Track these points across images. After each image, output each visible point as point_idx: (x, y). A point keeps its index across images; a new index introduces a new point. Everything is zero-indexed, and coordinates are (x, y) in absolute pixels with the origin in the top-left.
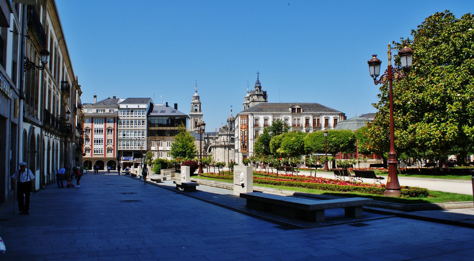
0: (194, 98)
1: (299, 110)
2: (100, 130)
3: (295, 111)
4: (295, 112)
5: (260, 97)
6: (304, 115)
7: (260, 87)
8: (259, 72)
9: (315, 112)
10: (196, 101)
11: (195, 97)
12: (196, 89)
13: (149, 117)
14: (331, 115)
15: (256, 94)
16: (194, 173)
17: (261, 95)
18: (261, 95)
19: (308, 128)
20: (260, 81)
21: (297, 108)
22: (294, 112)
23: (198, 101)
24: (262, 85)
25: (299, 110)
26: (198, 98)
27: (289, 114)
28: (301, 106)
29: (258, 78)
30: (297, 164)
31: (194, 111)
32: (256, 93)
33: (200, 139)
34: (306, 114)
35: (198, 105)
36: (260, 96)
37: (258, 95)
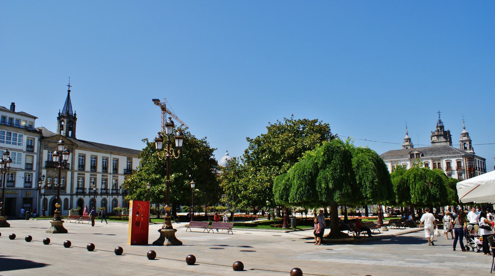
2: (482, 171)
5: (440, 138)
7: (442, 127)
8: (440, 111)
10: (408, 143)
11: (463, 134)
13: (30, 186)
14: (453, 157)
16: (257, 214)
18: (441, 135)
19: (450, 172)
20: (442, 120)
21: (416, 154)
23: (467, 138)
26: (467, 134)
27: (407, 160)
29: (439, 118)
31: (463, 149)
32: (436, 133)
33: (46, 194)
35: (468, 143)
36: (440, 136)
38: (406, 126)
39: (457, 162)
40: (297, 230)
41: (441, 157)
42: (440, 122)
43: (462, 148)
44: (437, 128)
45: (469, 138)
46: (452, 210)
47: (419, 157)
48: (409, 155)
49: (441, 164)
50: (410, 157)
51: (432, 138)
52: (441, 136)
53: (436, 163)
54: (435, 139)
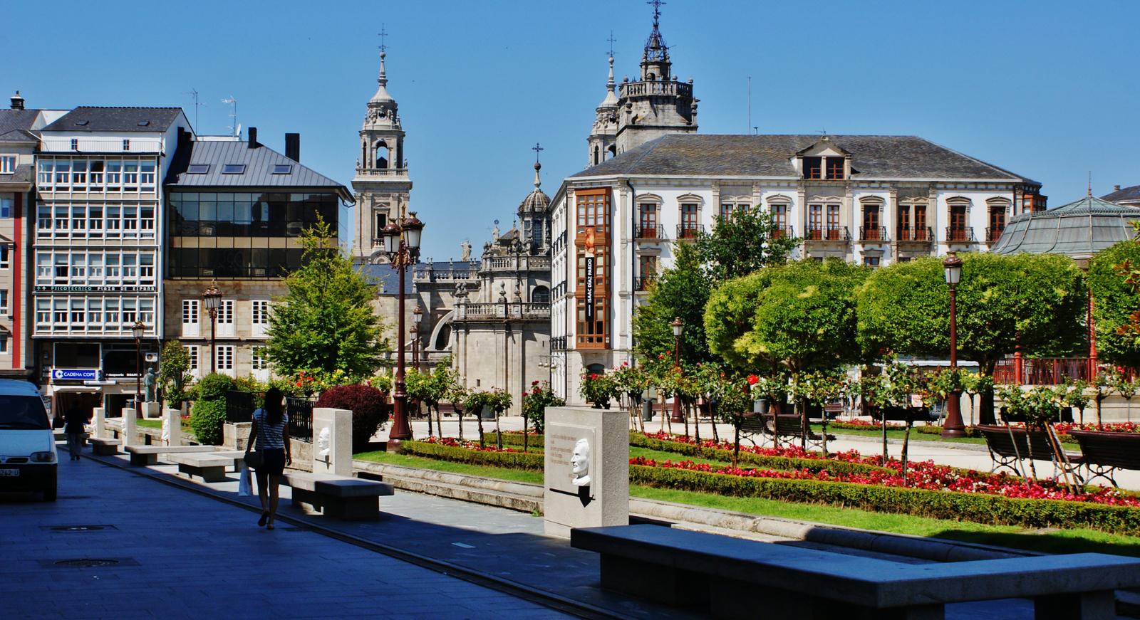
0: (374, 110)
1: (835, 168)
3: (819, 171)
4: (819, 176)
5: (663, 110)
7: (664, 66)
9: (906, 174)
10: (383, 123)
11: (378, 105)
17: (667, 100)
18: (667, 100)
19: (653, 245)
20: (667, 39)
21: (829, 159)
22: (815, 177)
23: (390, 123)
24: (672, 56)
25: (835, 168)
26: (389, 108)
27: (789, 186)
28: (843, 151)
29: (656, 26)
35: (392, 142)
36: (663, 103)
37: (654, 100)
39: (865, 206)
42: (657, 42)
43: (371, 164)
45: (398, 124)
46: (995, 404)
49: (928, 213)
52: (668, 103)
53: (908, 207)
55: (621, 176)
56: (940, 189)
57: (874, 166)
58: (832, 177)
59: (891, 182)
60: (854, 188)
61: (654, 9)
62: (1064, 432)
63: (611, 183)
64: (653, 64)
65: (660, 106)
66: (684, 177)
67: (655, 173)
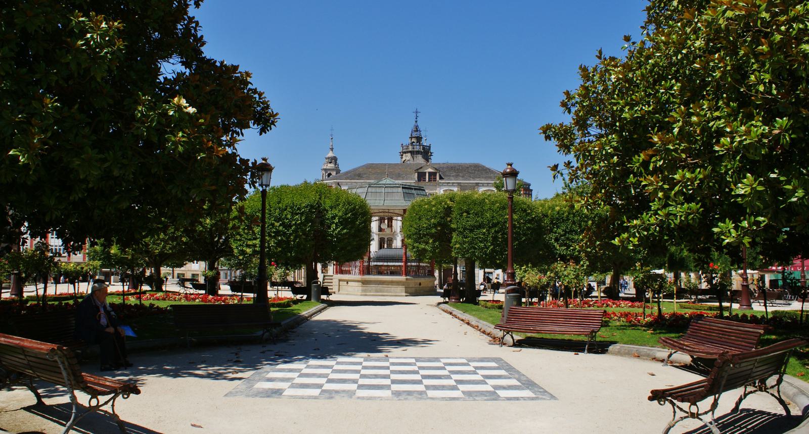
0: (327, 160)
1: (432, 177)
3: (425, 178)
4: (425, 181)
5: (416, 157)
6: (442, 185)
7: (419, 139)
8: (418, 110)
9: (466, 179)
10: (331, 166)
11: (329, 158)
12: (331, 144)
15: (410, 150)
17: (418, 152)
18: (418, 152)
20: (421, 127)
21: (429, 173)
22: (423, 181)
24: (423, 134)
25: (432, 177)
26: (334, 160)
28: (436, 169)
29: (416, 122)
30: (413, 272)
32: (410, 149)
34: (446, 184)
36: (416, 154)
37: (412, 153)
38: (332, 135)
40: (774, 305)
41: (477, 184)
42: (417, 129)
44: (411, 140)
47: (435, 179)
48: (416, 174)
50: (417, 179)
51: (402, 155)
52: (419, 154)
54: (408, 157)
55: (335, 181)
56: (481, 186)
57: (453, 176)
58: (431, 181)
59: (457, 183)
60: (440, 186)
61: (415, 115)
62: (188, 284)
63: (332, 184)
64: (414, 137)
65: (415, 155)
66: (363, 181)
67: (350, 180)
